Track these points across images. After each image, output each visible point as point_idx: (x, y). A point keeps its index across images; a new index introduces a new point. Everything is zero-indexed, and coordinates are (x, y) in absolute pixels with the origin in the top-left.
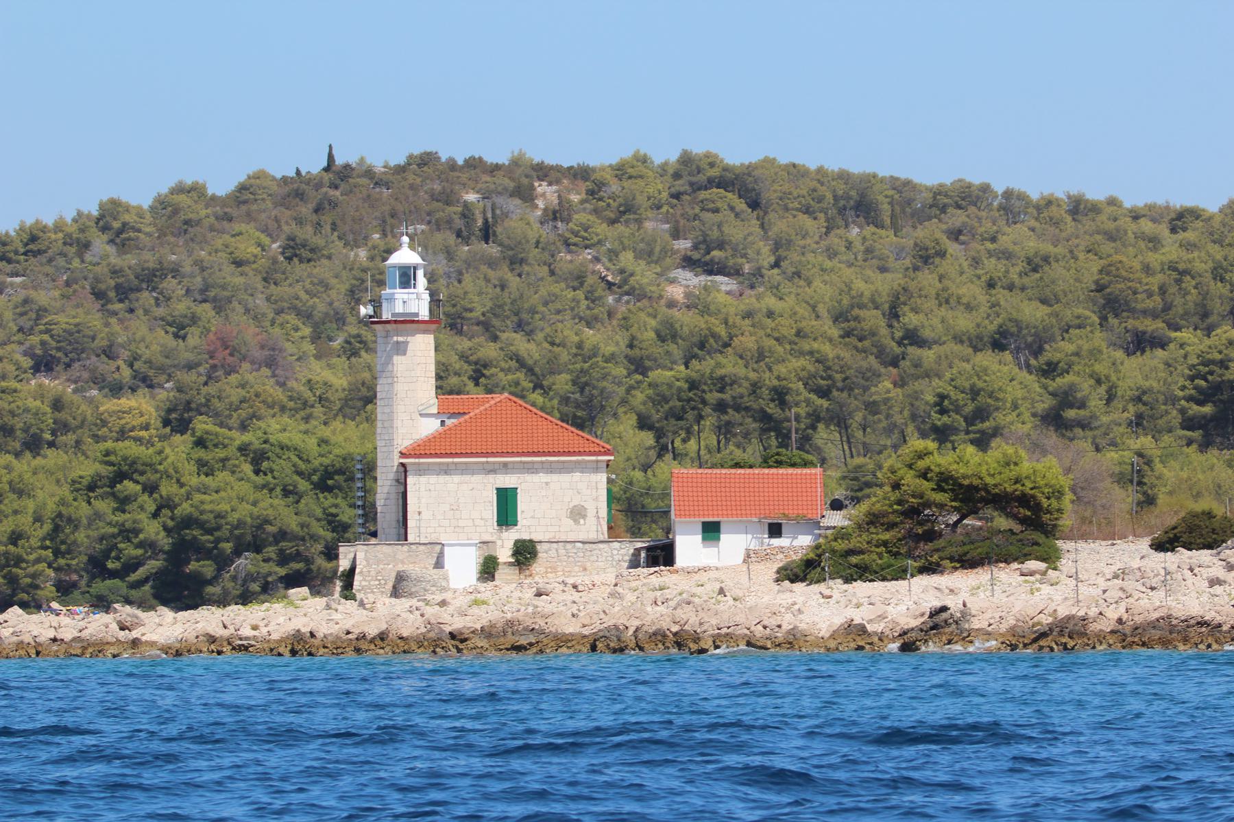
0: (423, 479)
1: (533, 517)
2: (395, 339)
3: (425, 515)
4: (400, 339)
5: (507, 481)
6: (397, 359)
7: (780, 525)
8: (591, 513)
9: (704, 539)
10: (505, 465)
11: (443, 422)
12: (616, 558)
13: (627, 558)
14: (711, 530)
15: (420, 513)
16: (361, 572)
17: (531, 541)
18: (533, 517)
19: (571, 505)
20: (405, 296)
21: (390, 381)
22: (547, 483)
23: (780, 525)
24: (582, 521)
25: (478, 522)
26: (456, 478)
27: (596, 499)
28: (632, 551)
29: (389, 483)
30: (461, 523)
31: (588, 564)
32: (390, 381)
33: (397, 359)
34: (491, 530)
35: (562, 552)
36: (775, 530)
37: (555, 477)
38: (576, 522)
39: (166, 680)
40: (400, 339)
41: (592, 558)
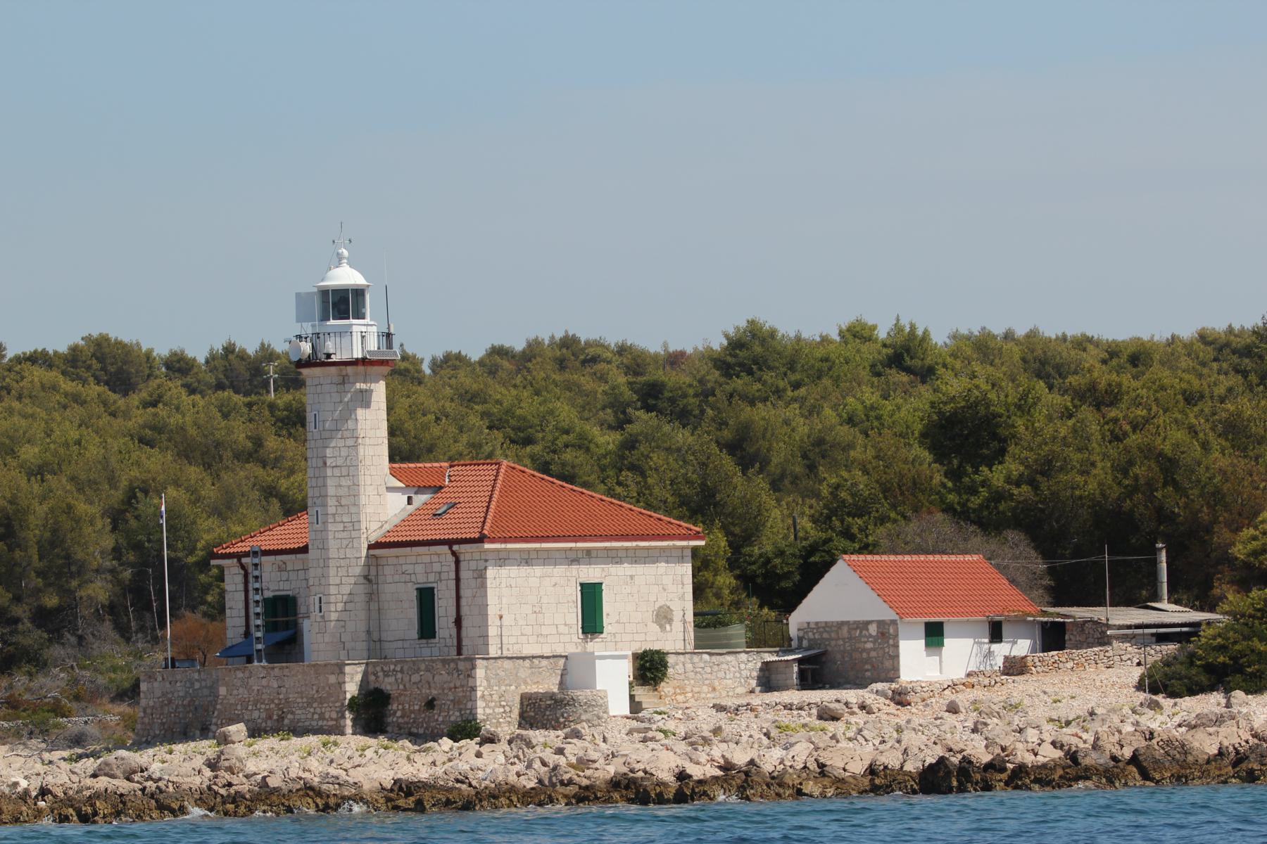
0: (504, 571)
1: (618, 622)
2: (358, 386)
3: (506, 621)
4: (363, 386)
5: (591, 573)
6: (360, 413)
7: (940, 625)
8: (677, 616)
9: (927, 645)
10: (588, 552)
11: (410, 499)
12: (745, 673)
13: (755, 674)
14: (934, 634)
15: (501, 617)
16: (483, 696)
17: (658, 652)
18: (618, 622)
19: (657, 606)
20: (364, 329)
21: (350, 442)
22: (632, 577)
23: (940, 625)
24: (668, 627)
25: (562, 629)
26: (538, 570)
27: (682, 598)
28: (759, 665)
29: (352, 580)
30: (545, 630)
31: (716, 683)
32: (350, 442)
33: (360, 413)
34: (575, 639)
35: (689, 666)
36: (996, 634)
37: (639, 569)
38: (662, 627)
39: (493, 830)
40: (363, 386)
41: (721, 674)
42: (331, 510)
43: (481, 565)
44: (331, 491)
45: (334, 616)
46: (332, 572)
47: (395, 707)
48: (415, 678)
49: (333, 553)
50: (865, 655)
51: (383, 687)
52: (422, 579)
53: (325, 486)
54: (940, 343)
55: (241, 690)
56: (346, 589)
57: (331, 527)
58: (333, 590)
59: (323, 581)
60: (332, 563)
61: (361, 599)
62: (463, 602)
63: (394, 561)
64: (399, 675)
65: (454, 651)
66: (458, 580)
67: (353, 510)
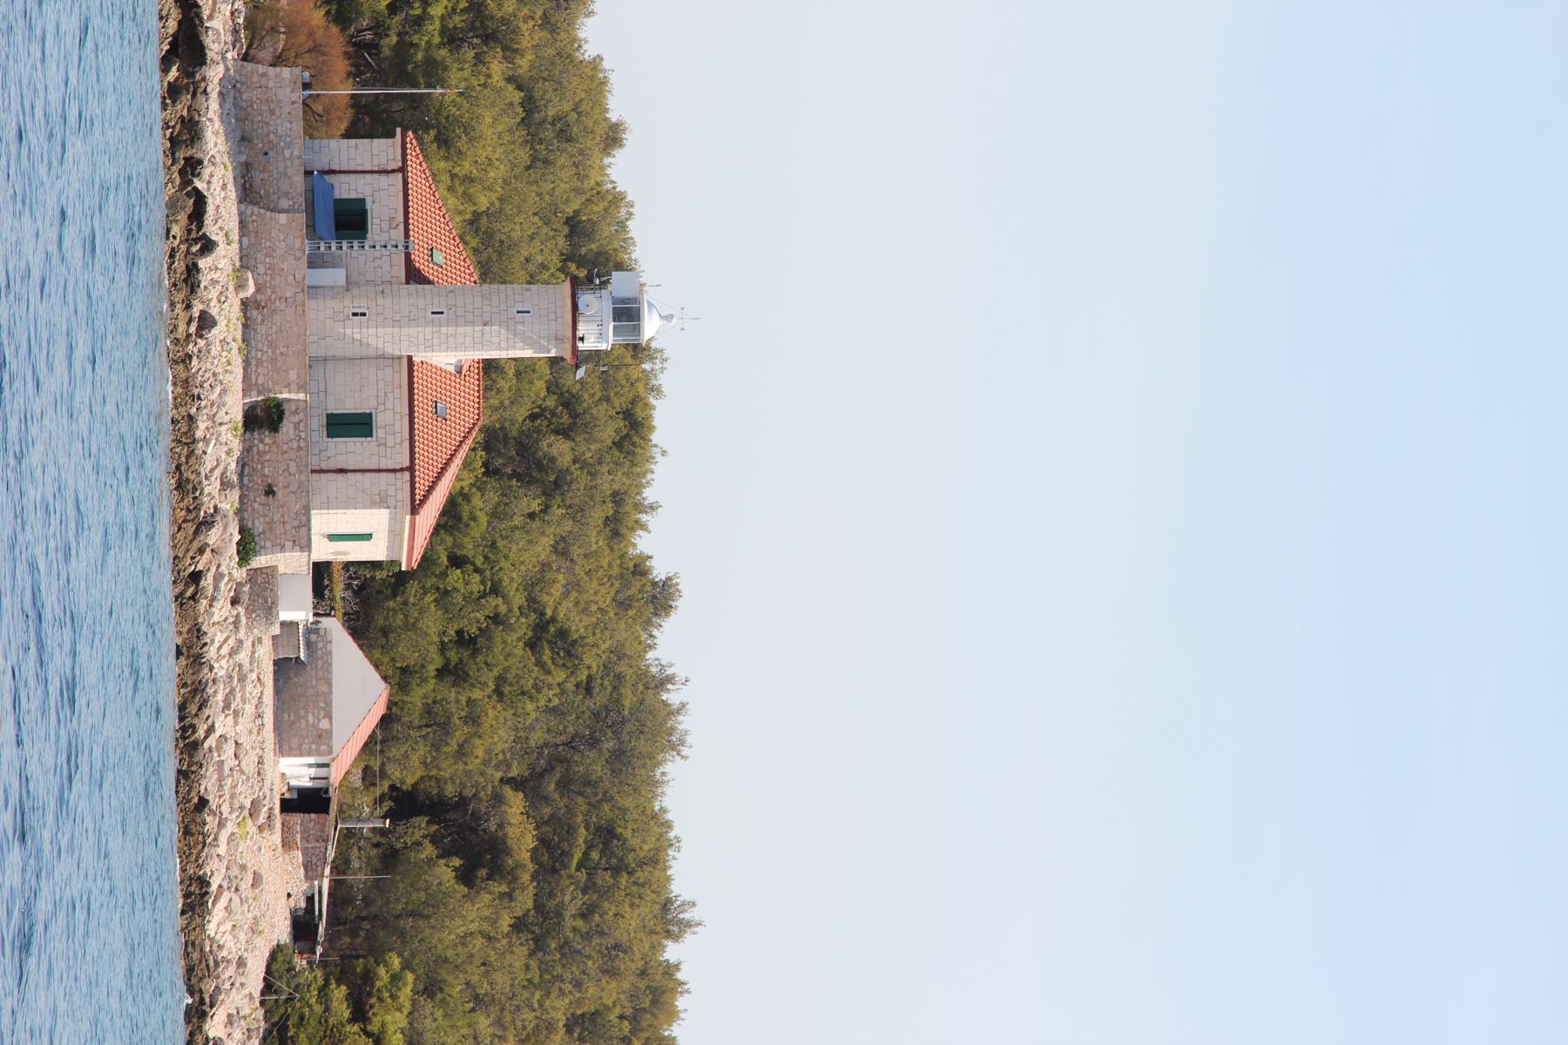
42: (444, 330)
43: (391, 502)
44: (461, 330)
45: (348, 331)
46: (389, 330)
47: (267, 440)
48: (293, 469)
49: (405, 331)
50: (302, 713)
51: (285, 422)
52: (379, 420)
53: (466, 323)
54: (637, 540)
55: (283, 245)
56: (372, 341)
57: (429, 329)
58: (372, 331)
59: (380, 318)
60: (396, 330)
61: (364, 352)
62: (359, 475)
63: (396, 383)
64: (295, 445)
65: (315, 465)
66: (379, 471)
67: (444, 347)
